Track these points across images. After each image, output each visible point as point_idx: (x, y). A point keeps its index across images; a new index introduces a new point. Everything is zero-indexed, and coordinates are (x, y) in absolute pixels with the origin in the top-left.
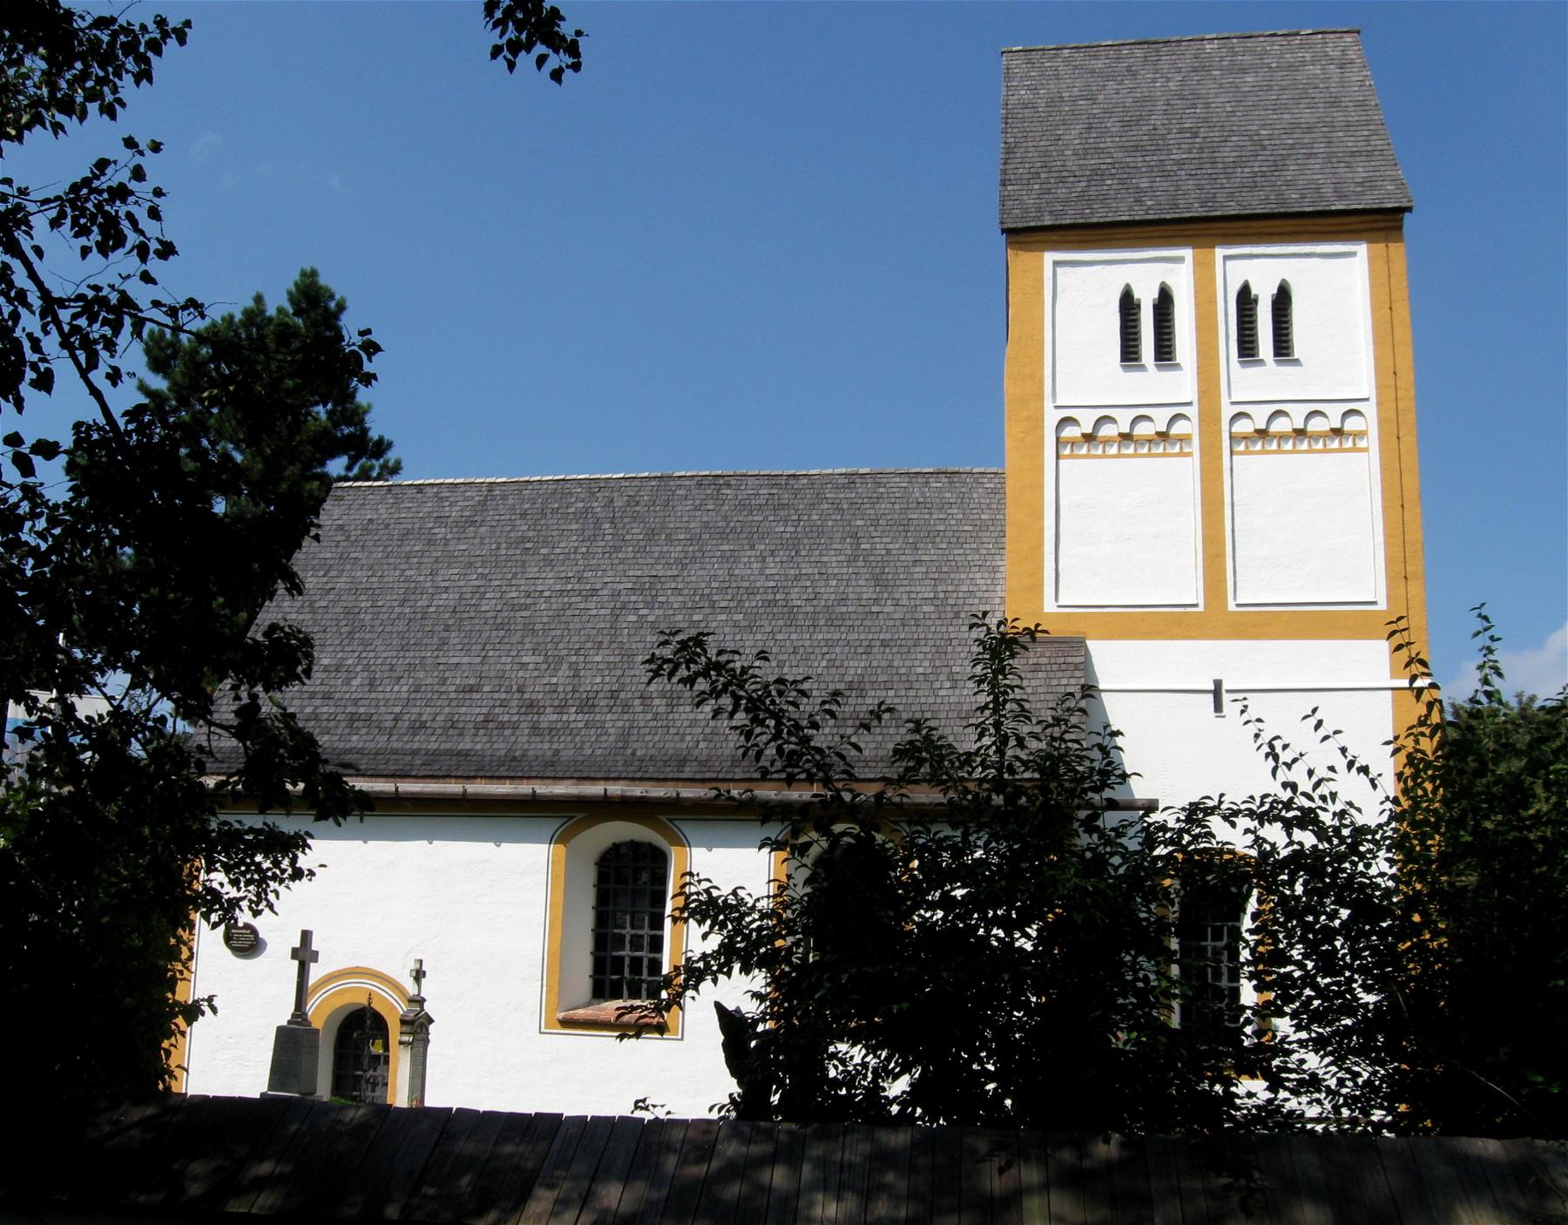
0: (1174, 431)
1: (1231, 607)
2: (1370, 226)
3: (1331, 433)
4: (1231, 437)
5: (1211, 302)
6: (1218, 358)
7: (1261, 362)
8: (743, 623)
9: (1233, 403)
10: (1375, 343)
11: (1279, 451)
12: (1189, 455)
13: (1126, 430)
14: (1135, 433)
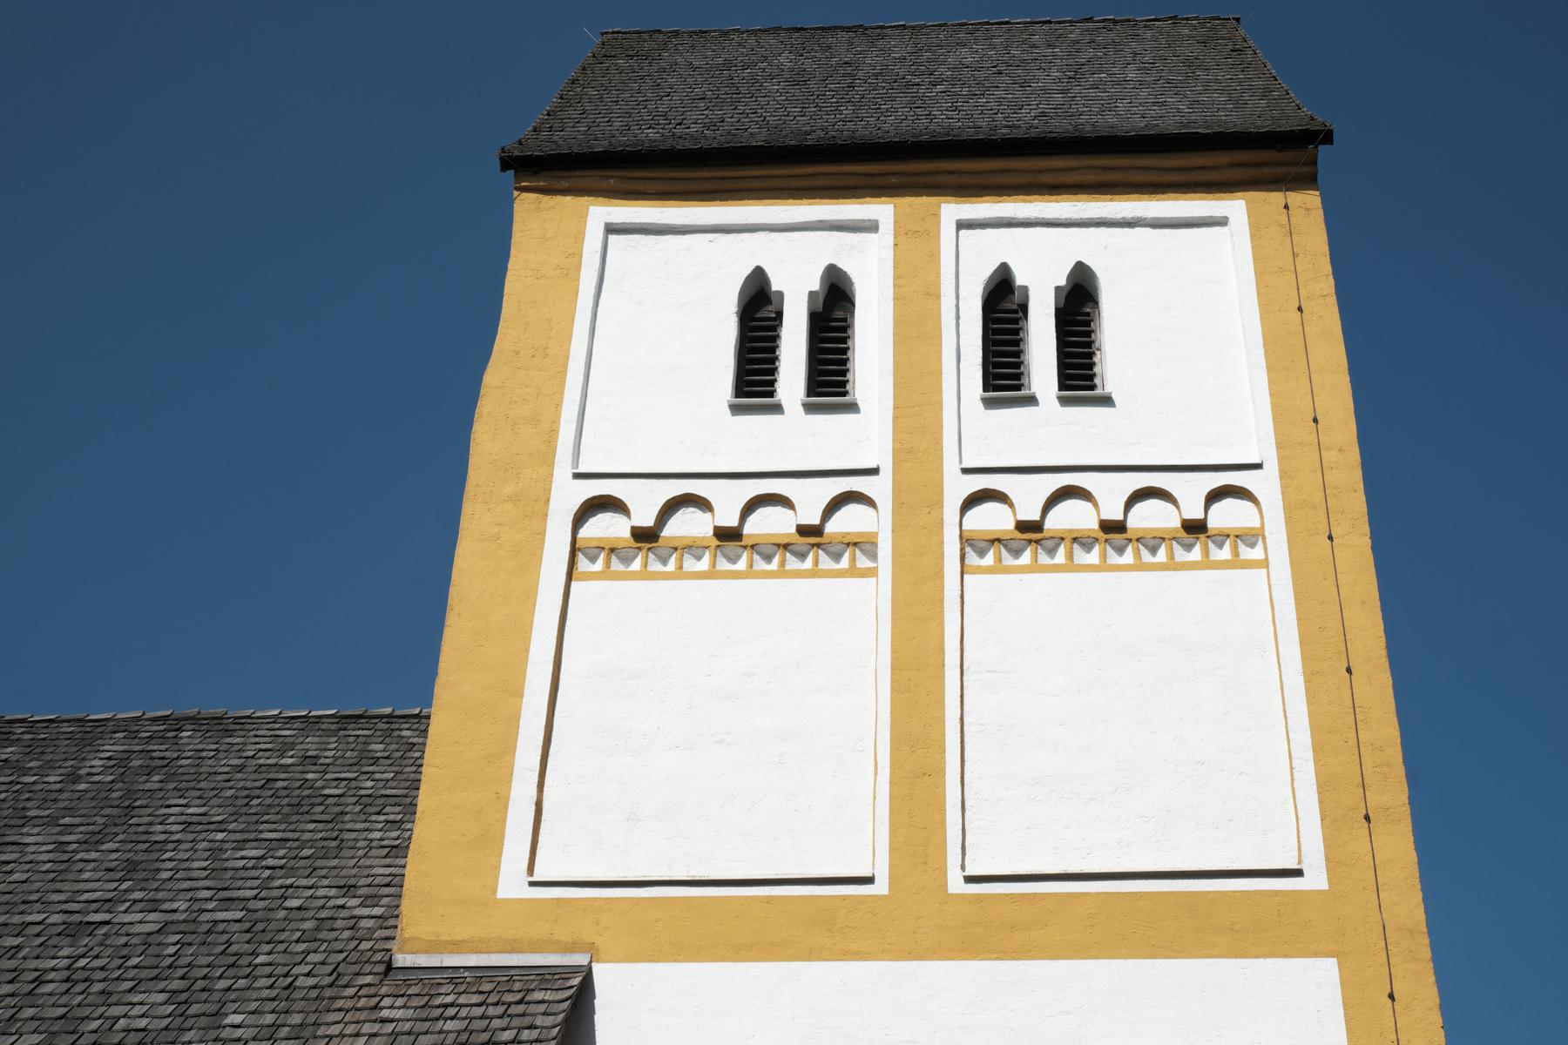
0: (832, 527)
1: (956, 884)
3: (1183, 534)
4: (966, 540)
6: (940, 391)
9: (966, 471)
10: (1270, 368)
13: (732, 521)
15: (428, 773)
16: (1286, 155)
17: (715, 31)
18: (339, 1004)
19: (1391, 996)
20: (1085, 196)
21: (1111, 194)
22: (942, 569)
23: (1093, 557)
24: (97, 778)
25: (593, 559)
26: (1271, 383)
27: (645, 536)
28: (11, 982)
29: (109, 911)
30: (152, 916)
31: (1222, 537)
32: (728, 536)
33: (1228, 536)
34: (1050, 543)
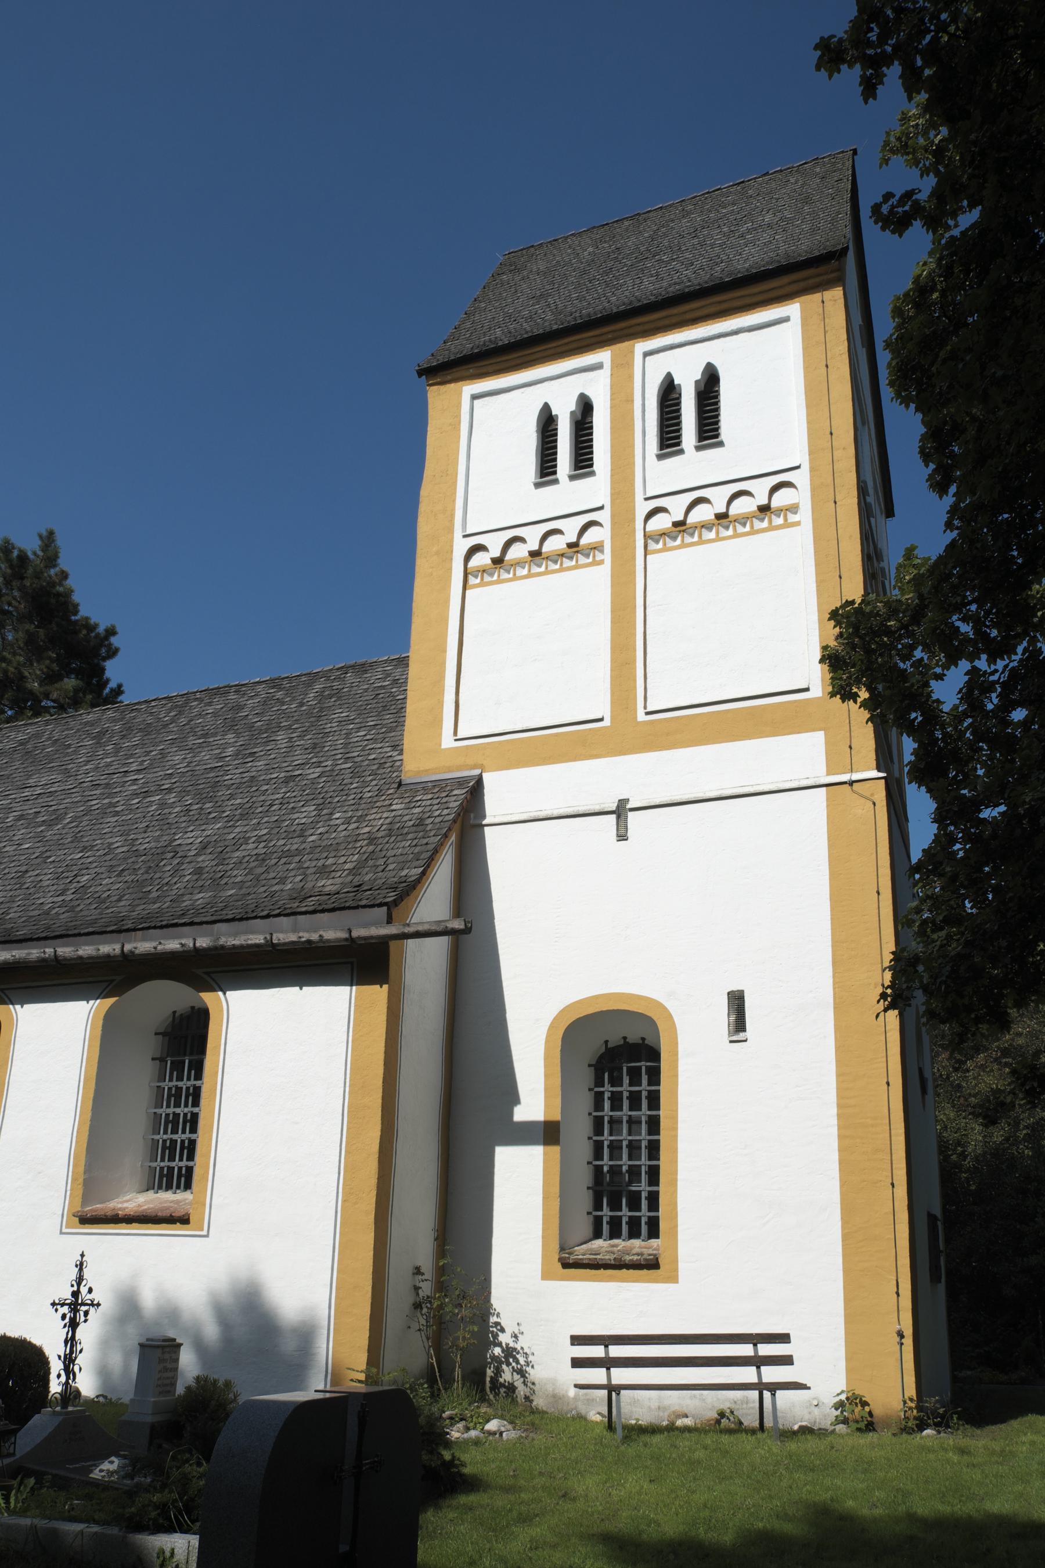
0: (583, 541)
1: (641, 716)
2: (817, 280)
4: (646, 536)
5: (628, 401)
6: (634, 456)
10: (808, 406)
12: (602, 562)
14: (544, 549)
15: (410, 694)
16: (822, 269)
17: (561, 238)
18: (378, 804)
19: (850, 747)
20: (711, 322)
21: (725, 317)
22: (635, 555)
23: (712, 535)
24: (310, 703)
25: (476, 577)
26: (808, 415)
27: (498, 561)
28: (261, 806)
29: (302, 769)
30: (318, 770)
31: (779, 511)
32: (535, 554)
33: (782, 510)
34: (691, 531)
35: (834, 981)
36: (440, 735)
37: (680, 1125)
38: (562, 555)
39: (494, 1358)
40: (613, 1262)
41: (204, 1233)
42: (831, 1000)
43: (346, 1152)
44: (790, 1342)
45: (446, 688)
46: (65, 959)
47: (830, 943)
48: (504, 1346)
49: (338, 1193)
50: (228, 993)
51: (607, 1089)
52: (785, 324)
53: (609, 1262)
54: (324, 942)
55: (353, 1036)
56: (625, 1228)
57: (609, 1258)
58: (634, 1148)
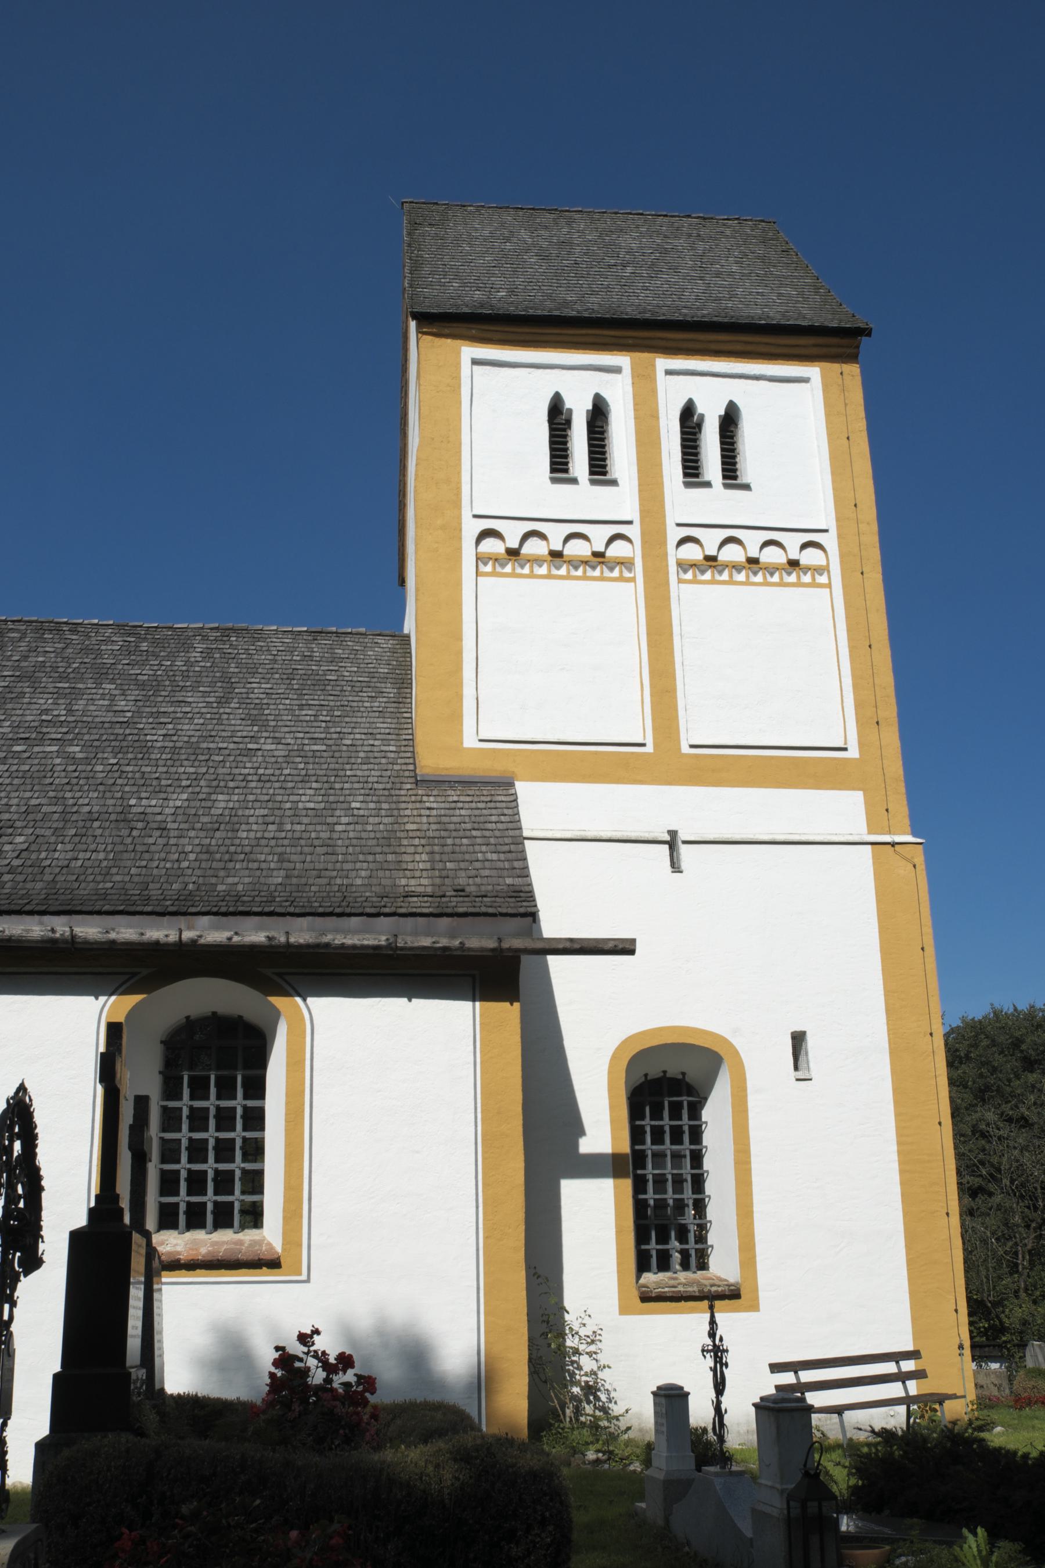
3: (787, 566)
7: (574, 481)
8: (80, 755)
11: (731, 582)
14: (524, 551)
31: (807, 569)
35: (888, 1028)
36: (461, 731)
37: (753, 1159)
38: (586, 563)
39: (574, 1398)
40: (697, 1294)
41: (304, 1277)
42: (887, 1046)
43: (483, 1184)
44: (921, 1358)
45: (465, 681)
46: (86, 942)
47: (882, 992)
48: (583, 1384)
49: (477, 1229)
50: (309, 1000)
51: (647, 1123)
52: (803, 384)
53: (693, 1294)
54: (464, 951)
55: (481, 1058)
56: (654, 1261)
57: (694, 1289)
58: (678, 1181)
